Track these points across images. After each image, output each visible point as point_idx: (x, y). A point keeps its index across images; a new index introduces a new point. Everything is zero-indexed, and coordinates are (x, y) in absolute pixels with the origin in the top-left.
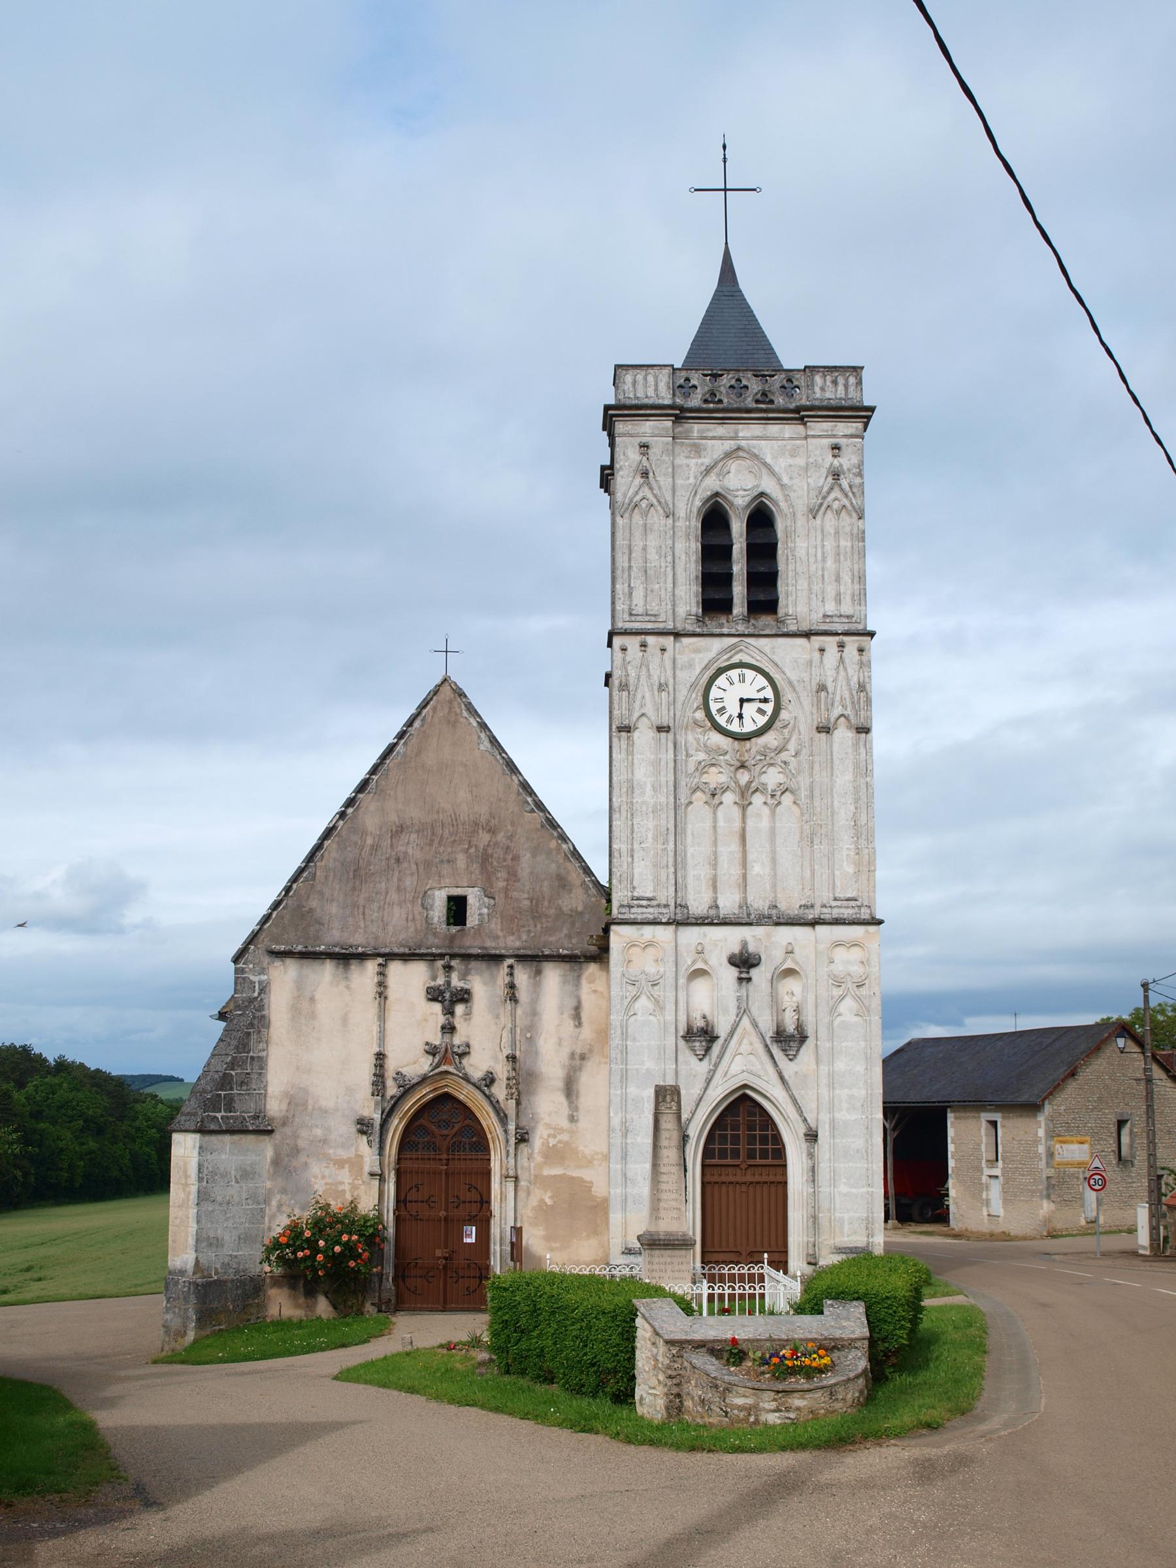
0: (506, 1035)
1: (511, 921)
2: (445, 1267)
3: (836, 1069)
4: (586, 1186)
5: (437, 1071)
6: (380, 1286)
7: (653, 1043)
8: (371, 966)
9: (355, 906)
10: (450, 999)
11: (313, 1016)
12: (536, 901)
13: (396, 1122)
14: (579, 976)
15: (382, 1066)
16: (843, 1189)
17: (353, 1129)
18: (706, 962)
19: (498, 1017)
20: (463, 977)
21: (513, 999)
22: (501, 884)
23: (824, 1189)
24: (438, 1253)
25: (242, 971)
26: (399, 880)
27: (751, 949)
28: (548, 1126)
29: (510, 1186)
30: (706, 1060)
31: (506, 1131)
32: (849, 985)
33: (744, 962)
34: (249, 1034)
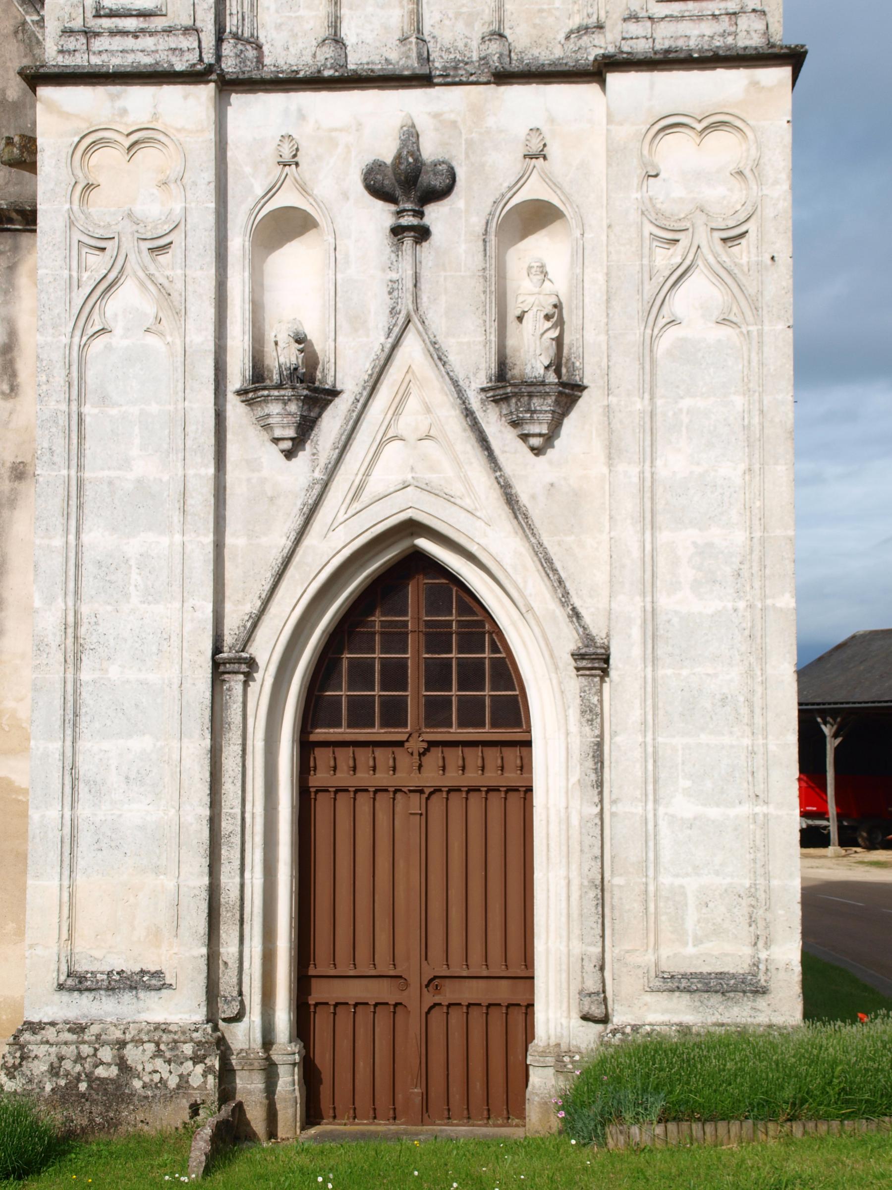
3: (662, 472)
7: (154, 408)
16: (680, 805)
18: (303, 189)
23: (626, 805)
27: (429, 151)
30: (303, 457)
32: (702, 236)
33: (410, 187)
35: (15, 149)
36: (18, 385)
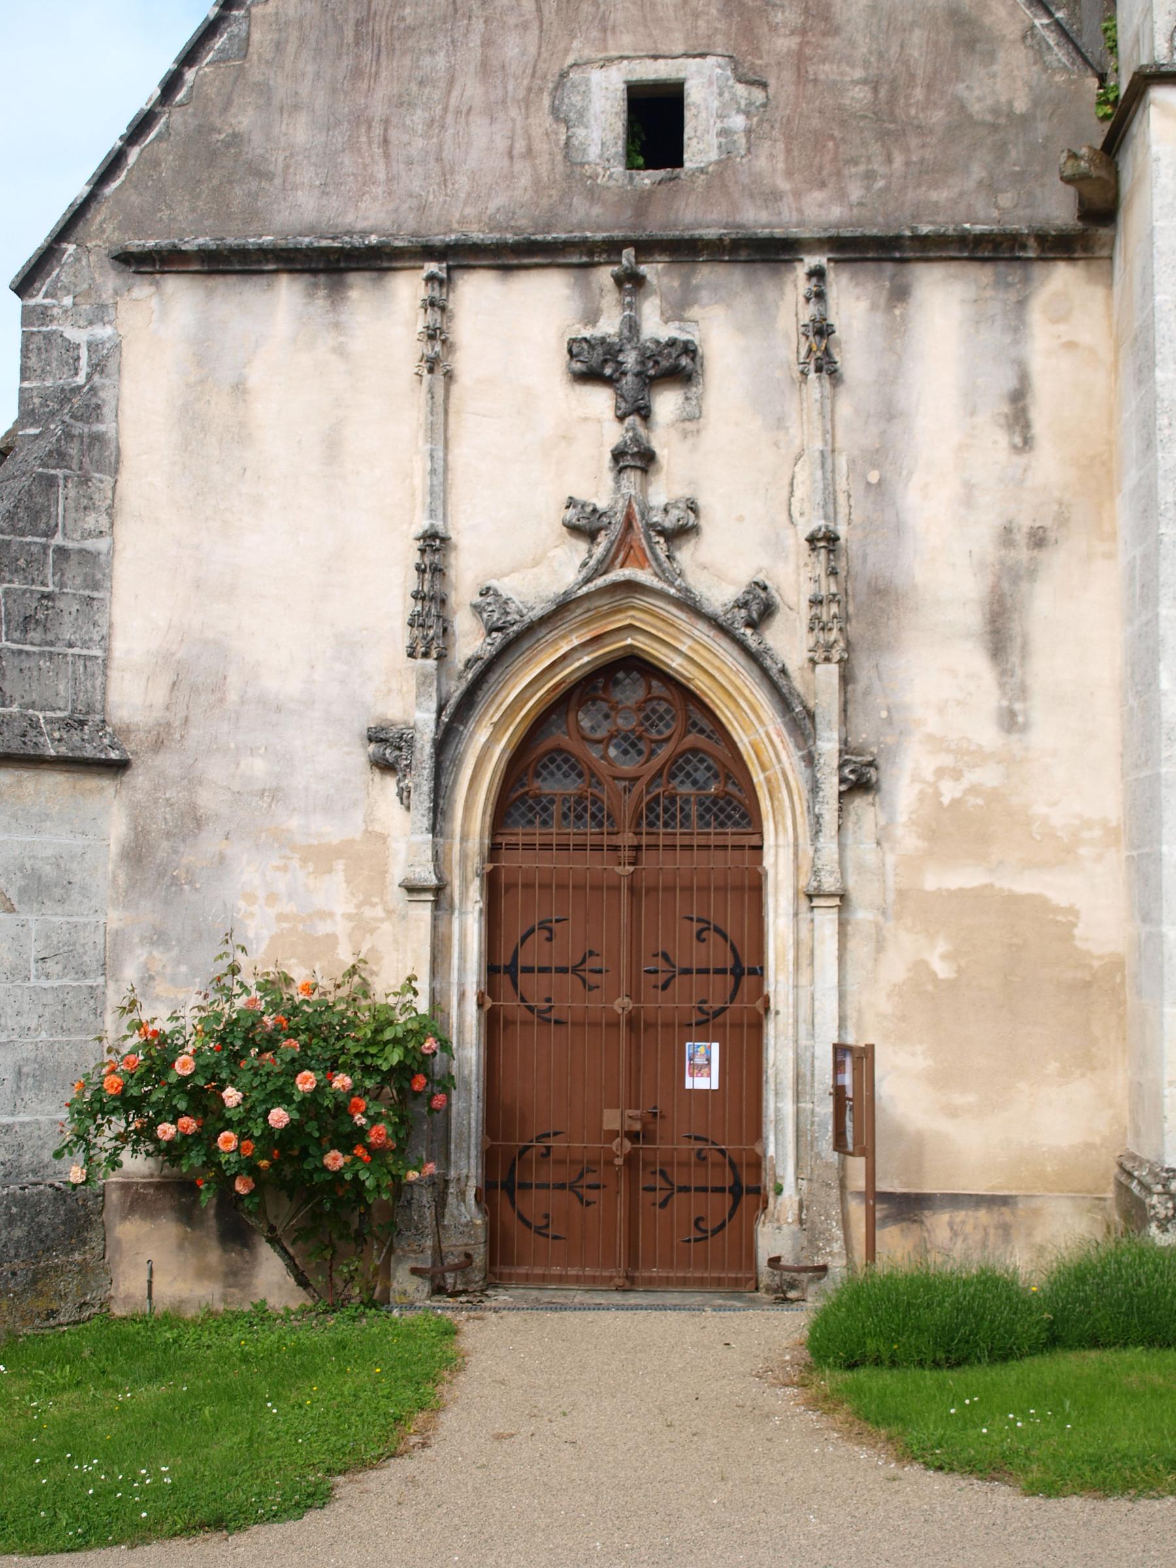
0: (807, 477)
1: (818, 147)
2: (631, 1160)
4: (1057, 924)
5: (600, 582)
6: (439, 1216)
8: (408, 288)
9: (360, 119)
10: (639, 375)
11: (241, 435)
12: (888, 88)
13: (482, 735)
14: (1022, 304)
15: (438, 571)
17: (359, 755)
19: (780, 423)
20: (676, 311)
21: (825, 365)
22: (784, 43)
24: (612, 1120)
25: (44, 314)
26: (487, 43)
28: (936, 743)
29: (826, 921)
31: (810, 760)
34: (51, 482)
35: (1082, 163)
36: (1032, 438)
